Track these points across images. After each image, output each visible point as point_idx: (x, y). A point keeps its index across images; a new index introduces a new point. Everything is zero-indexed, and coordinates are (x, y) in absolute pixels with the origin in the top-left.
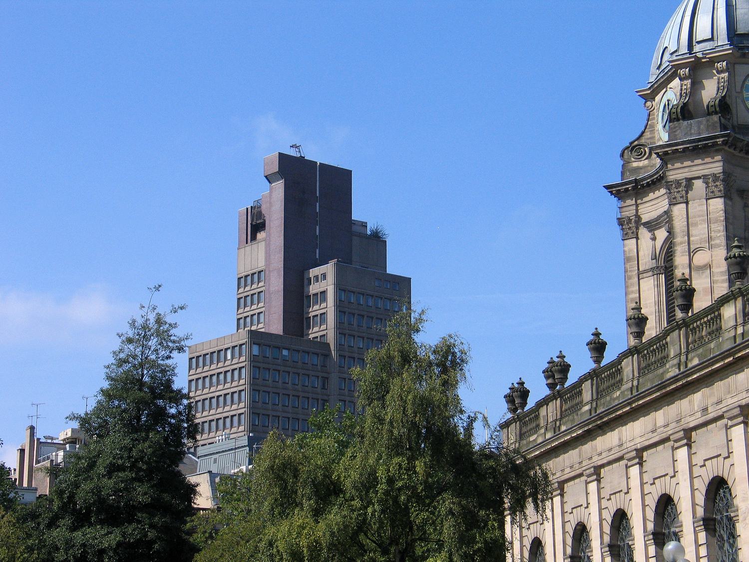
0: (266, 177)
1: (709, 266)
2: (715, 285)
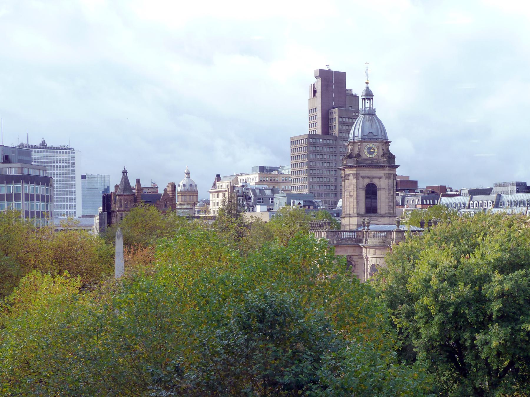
1: (353, 196)
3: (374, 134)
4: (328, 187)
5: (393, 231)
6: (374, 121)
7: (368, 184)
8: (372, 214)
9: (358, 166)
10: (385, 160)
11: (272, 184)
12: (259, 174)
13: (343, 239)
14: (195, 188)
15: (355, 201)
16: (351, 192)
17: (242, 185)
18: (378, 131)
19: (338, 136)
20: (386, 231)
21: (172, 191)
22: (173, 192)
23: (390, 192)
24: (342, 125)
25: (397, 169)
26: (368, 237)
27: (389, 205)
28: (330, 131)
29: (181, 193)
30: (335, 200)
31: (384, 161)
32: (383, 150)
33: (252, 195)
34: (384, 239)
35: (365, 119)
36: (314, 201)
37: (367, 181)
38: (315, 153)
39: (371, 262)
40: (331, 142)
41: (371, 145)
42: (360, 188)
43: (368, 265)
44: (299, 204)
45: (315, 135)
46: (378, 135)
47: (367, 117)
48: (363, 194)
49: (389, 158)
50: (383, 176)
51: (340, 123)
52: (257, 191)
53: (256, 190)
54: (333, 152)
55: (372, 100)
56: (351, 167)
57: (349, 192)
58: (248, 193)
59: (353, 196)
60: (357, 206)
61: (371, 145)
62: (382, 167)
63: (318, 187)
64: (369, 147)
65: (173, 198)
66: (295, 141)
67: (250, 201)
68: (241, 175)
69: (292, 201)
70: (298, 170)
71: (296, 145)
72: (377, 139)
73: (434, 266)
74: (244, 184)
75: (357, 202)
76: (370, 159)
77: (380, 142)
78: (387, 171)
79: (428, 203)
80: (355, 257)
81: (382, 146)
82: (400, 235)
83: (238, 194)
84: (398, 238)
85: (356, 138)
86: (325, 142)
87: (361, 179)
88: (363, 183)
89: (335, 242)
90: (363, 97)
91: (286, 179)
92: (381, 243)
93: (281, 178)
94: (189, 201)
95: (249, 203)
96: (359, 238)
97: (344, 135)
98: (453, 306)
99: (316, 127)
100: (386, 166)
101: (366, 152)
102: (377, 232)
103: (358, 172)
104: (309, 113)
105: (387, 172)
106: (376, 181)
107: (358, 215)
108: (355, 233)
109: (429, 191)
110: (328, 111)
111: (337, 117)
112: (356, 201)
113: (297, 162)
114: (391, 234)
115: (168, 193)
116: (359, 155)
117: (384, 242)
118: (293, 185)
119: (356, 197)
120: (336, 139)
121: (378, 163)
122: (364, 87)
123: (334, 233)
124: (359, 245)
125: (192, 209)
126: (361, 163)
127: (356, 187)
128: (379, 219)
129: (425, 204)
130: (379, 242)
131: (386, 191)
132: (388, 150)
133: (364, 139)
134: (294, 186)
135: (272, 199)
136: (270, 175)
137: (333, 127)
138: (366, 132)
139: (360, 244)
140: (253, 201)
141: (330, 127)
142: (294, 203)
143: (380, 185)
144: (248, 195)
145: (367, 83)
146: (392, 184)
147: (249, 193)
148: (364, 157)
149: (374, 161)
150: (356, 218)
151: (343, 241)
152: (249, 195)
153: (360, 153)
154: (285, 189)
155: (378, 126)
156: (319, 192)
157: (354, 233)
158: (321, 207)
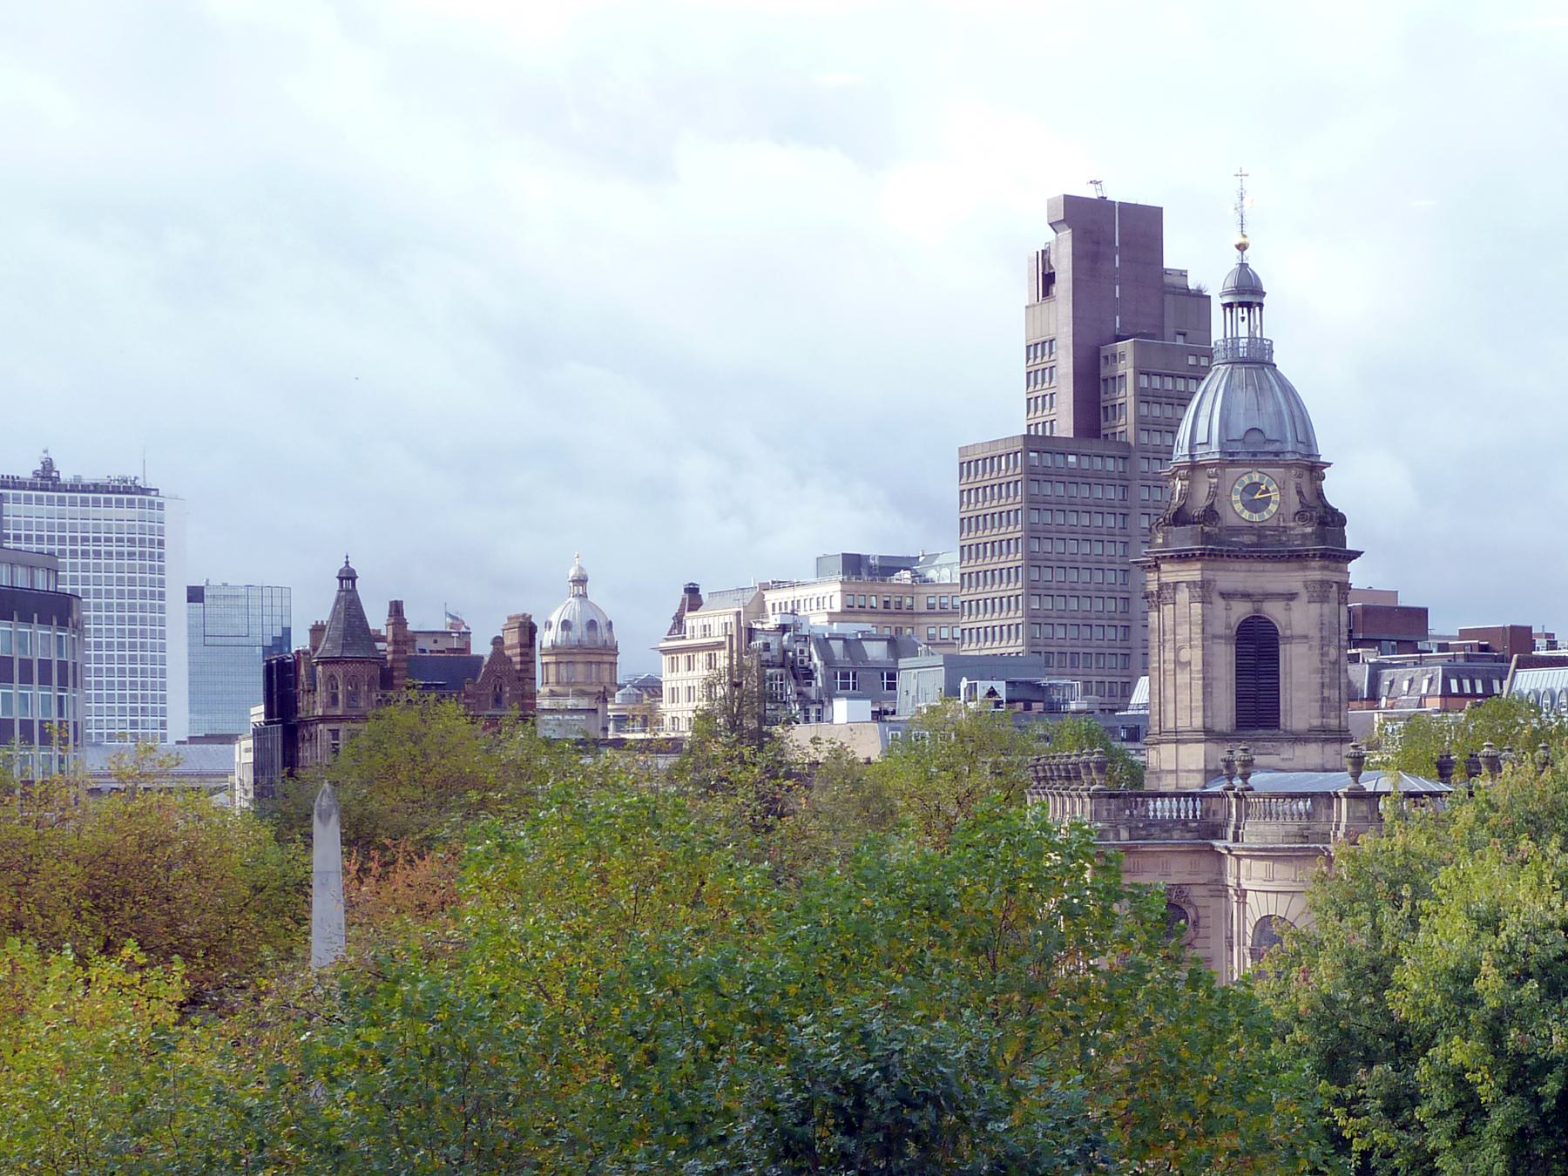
0: (1051, 225)
1: (1189, 663)
2: (1193, 682)
3: (1268, 435)
4: (1098, 632)
5: (1336, 793)
6: (1267, 385)
7: (1245, 621)
8: (1261, 731)
9: (1209, 555)
10: (1309, 530)
11: (892, 619)
12: (842, 582)
13: (1151, 825)
14: (606, 635)
15: (1198, 685)
16: (1181, 648)
17: (779, 622)
18: (1281, 424)
19: (1133, 443)
20: (1313, 795)
21: (522, 646)
22: (527, 650)
23: (1325, 649)
24: (1160, 404)
25: (1352, 566)
26: (1247, 815)
27: (1323, 700)
28: (1103, 424)
29: (556, 654)
30: (1125, 680)
31: (1304, 536)
32: (1300, 493)
33: (816, 659)
34: (1304, 822)
35: (1236, 380)
36: (1045, 681)
37: (1241, 610)
38: (1048, 506)
39: (1258, 907)
40: (1110, 464)
41: (1256, 478)
42: (1215, 637)
43: (1245, 918)
44: (992, 693)
45: (1051, 438)
46: (1282, 441)
47: (1241, 371)
48: (1225, 656)
49: (1322, 523)
50: (1302, 591)
51: (1143, 396)
52: (837, 646)
53: (831, 642)
54: (1116, 503)
55: (1261, 310)
56: (1182, 557)
57: (1177, 651)
58: (802, 652)
59: (1189, 663)
60: (1204, 700)
61: (1258, 475)
62: (1297, 557)
63: (1060, 633)
64: (1247, 482)
65: (527, 670)
66: (977, 461)
67: (810, 684)
68: (778, 585)
69: (964, 683)
70: (985, 568)
71: (979, 478)
72: (1277, 454)
73: (1490, 922)
74: (789, 620)
75: (1205, 687)
76: (1251, 528)
77: (1288, 466)
78: (1315, 572)
79: (1468, 690)
80: (1196, 891)
81: (1298, 480)
82: (1363, 808)
83: (766, 656)
84: (1358, 818)
85: (1199, 450)
86: (1085, 463)
87: (1220, 603)
88: (1228, 617)
89: (1124, 834)
90: (1227, 300)
91: (944, 600)
92: (1292, 839)
93: (923, 598)
94: (585, 684)
95: (805, 689)
96: (1211, 819)
97: (1157, 439)
98: (1559, 1071)
99: (1053, 410)
100: (1311, 553)
101: (1237, 502)
102: (1277, 796)
103: (1209, 575)
104: (1028, 359)
105: (1317, 575)
106: (1273, 611)
107: (1210, 735)
108: (1198, 802)
109: (1471, 645)
110: (1098, 351)
111: (1130, 373)
112: (1200, 682)
113: (985, 540)
114: (1330, 807)
115: (508, 653)
116: (1211, 514)
117: (1303, 836)
118: (967, 622)
119: (1200, 668)
120: (1125, 453)
121: (1283, 544)
122: (1232, 260)
123: (1121, 800)
124: (1212, 846)
125: (595, 711)
126: (1218, 544)
127: (1199, 631)
128: (1287, 751)
129: (1455, 695)
130: (1287, 835)
131: (1310, 647)
132: (1320, 495)
133: (1232, 454)
134: (970, 626)
135: (892, 676)
136: (883, 589)
137: (1115, 410)
138: (1239, 428)
139: (1216, 843)
140: (820, 684)
141: (1106, 408)
142: (972, 689)
143: (1289, 626)
144: (802, 661)
145: (1242, 247)
146: (1336, 621)
147: (806, 654)
148: (1230, 520)
149: (1266, 536)
150: (1202, 745)
151: (1153, 830)
152: (806, 660)
153: (1216, 507)
154: (938, 641)
155: (1284, 407)
156: (1064, 650)
157: (1194, 801)
158: (1073, 706)
